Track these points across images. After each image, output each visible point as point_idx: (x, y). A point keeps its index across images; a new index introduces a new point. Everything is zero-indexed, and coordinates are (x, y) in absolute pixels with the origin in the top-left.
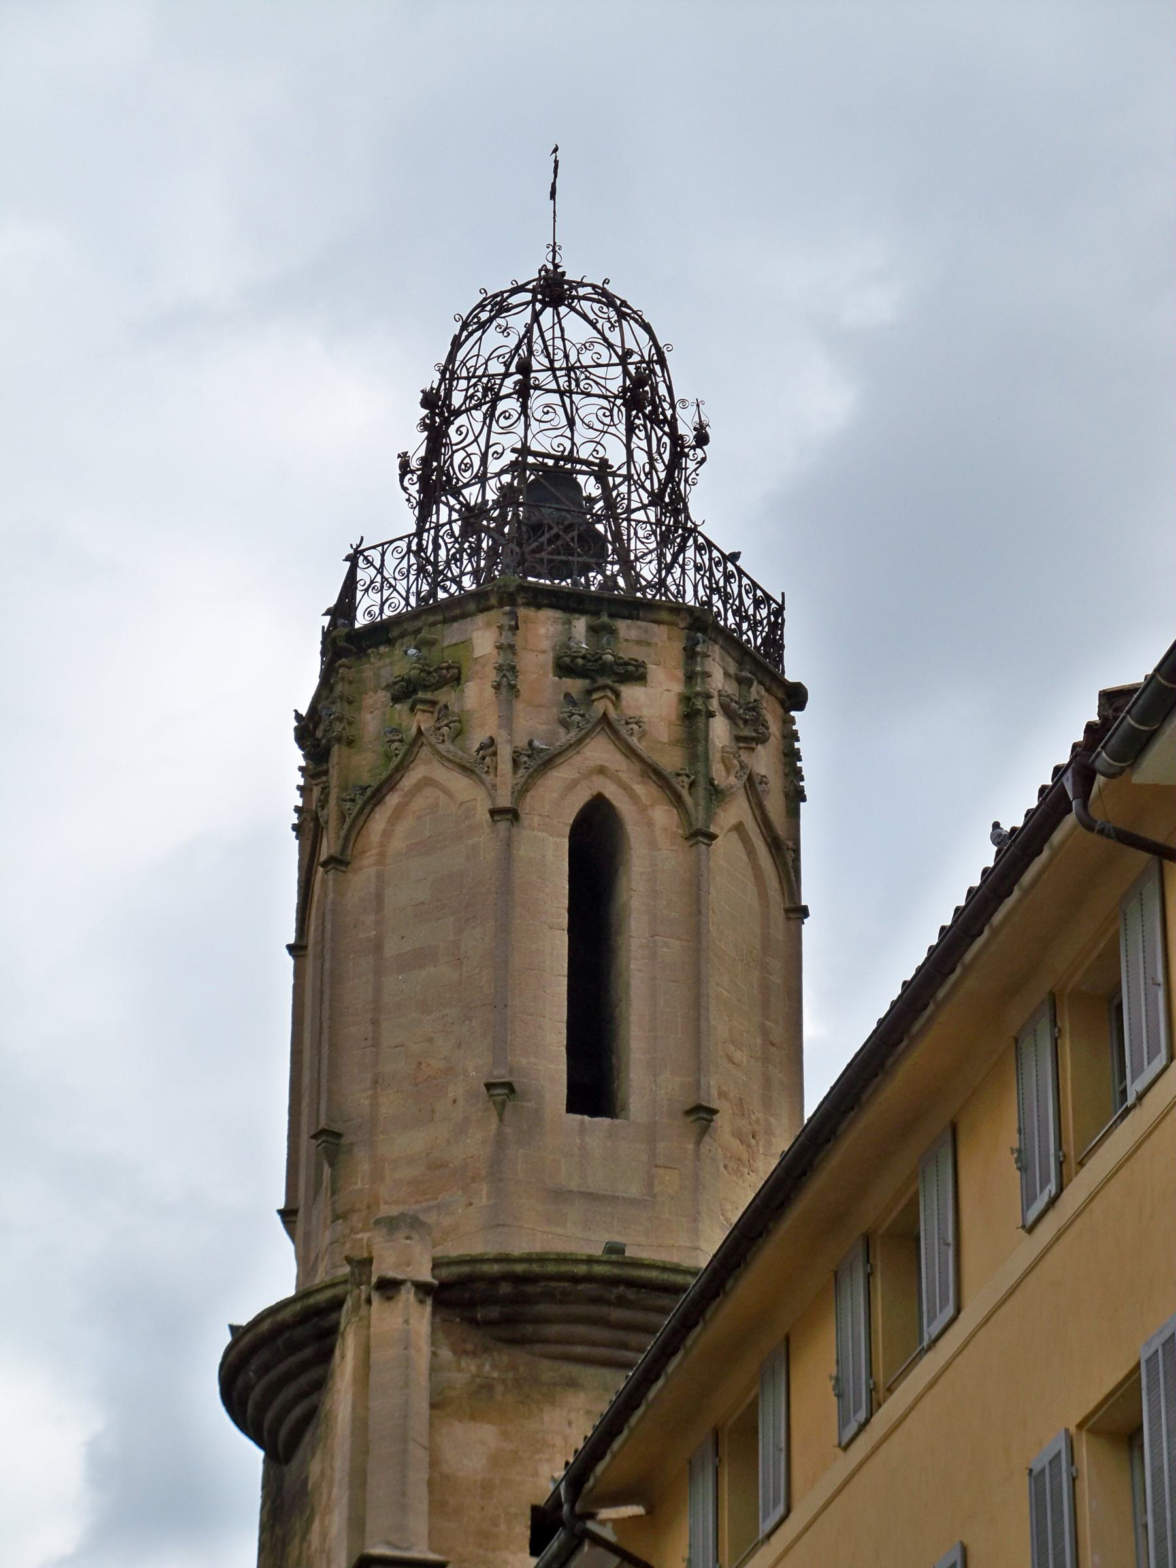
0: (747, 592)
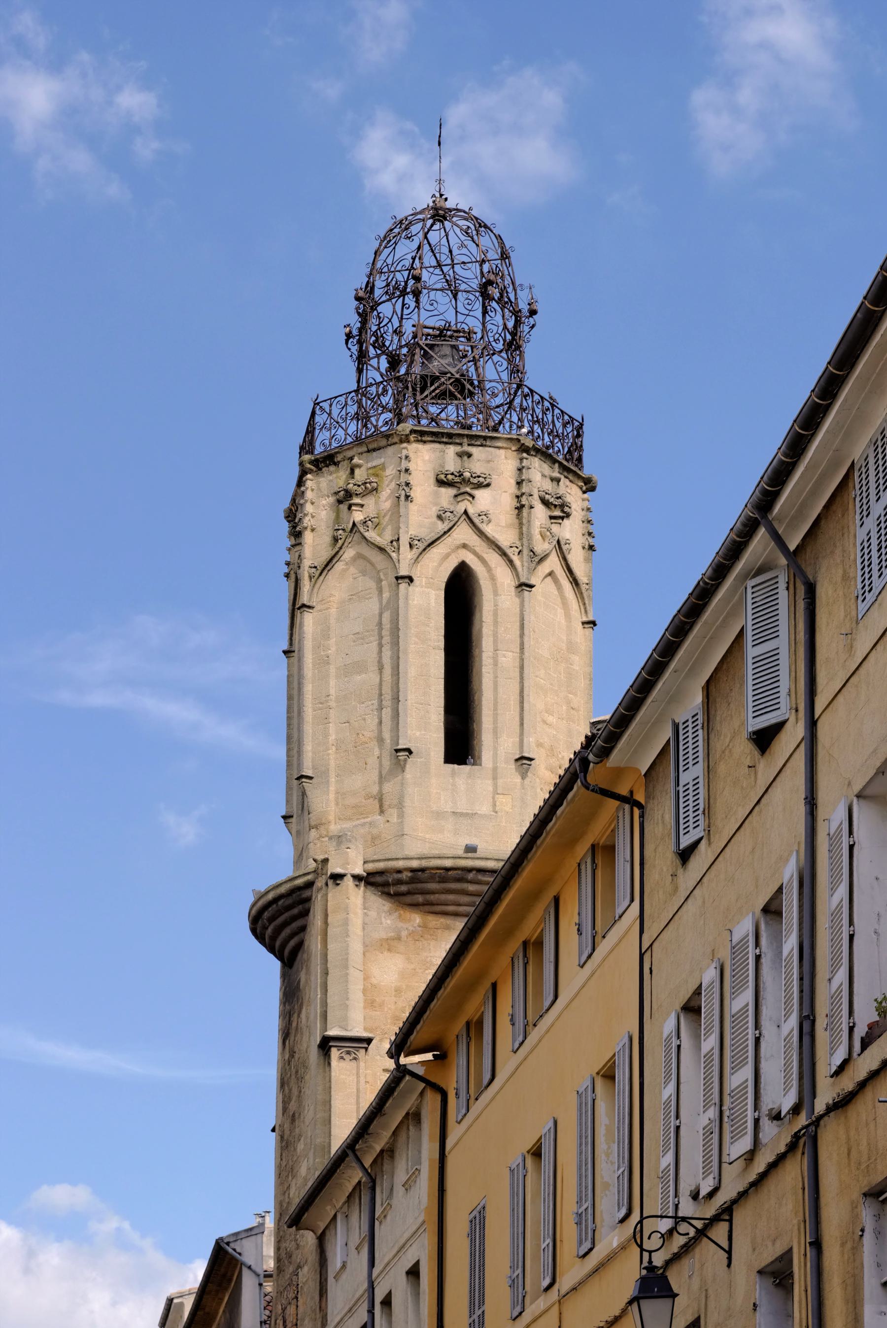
0: (558, 418)
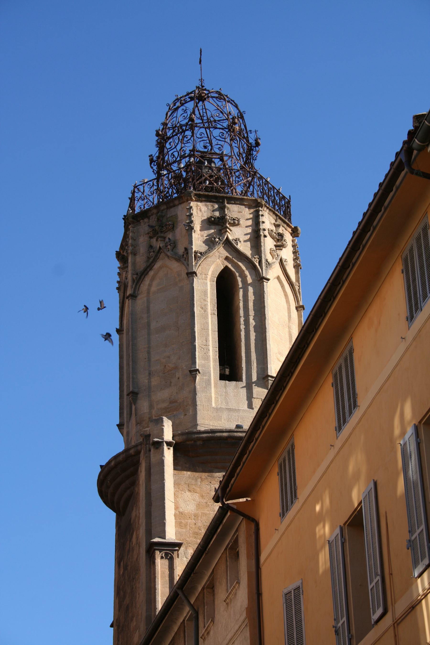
0: (277, 195)
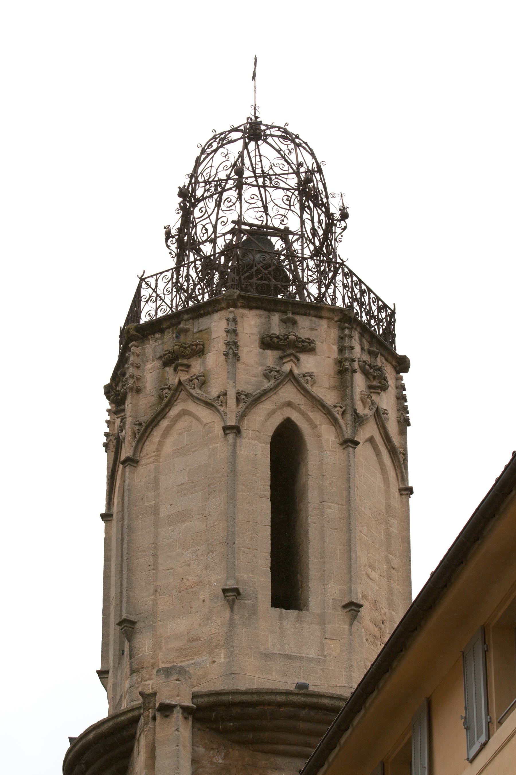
0: (374, 302)
